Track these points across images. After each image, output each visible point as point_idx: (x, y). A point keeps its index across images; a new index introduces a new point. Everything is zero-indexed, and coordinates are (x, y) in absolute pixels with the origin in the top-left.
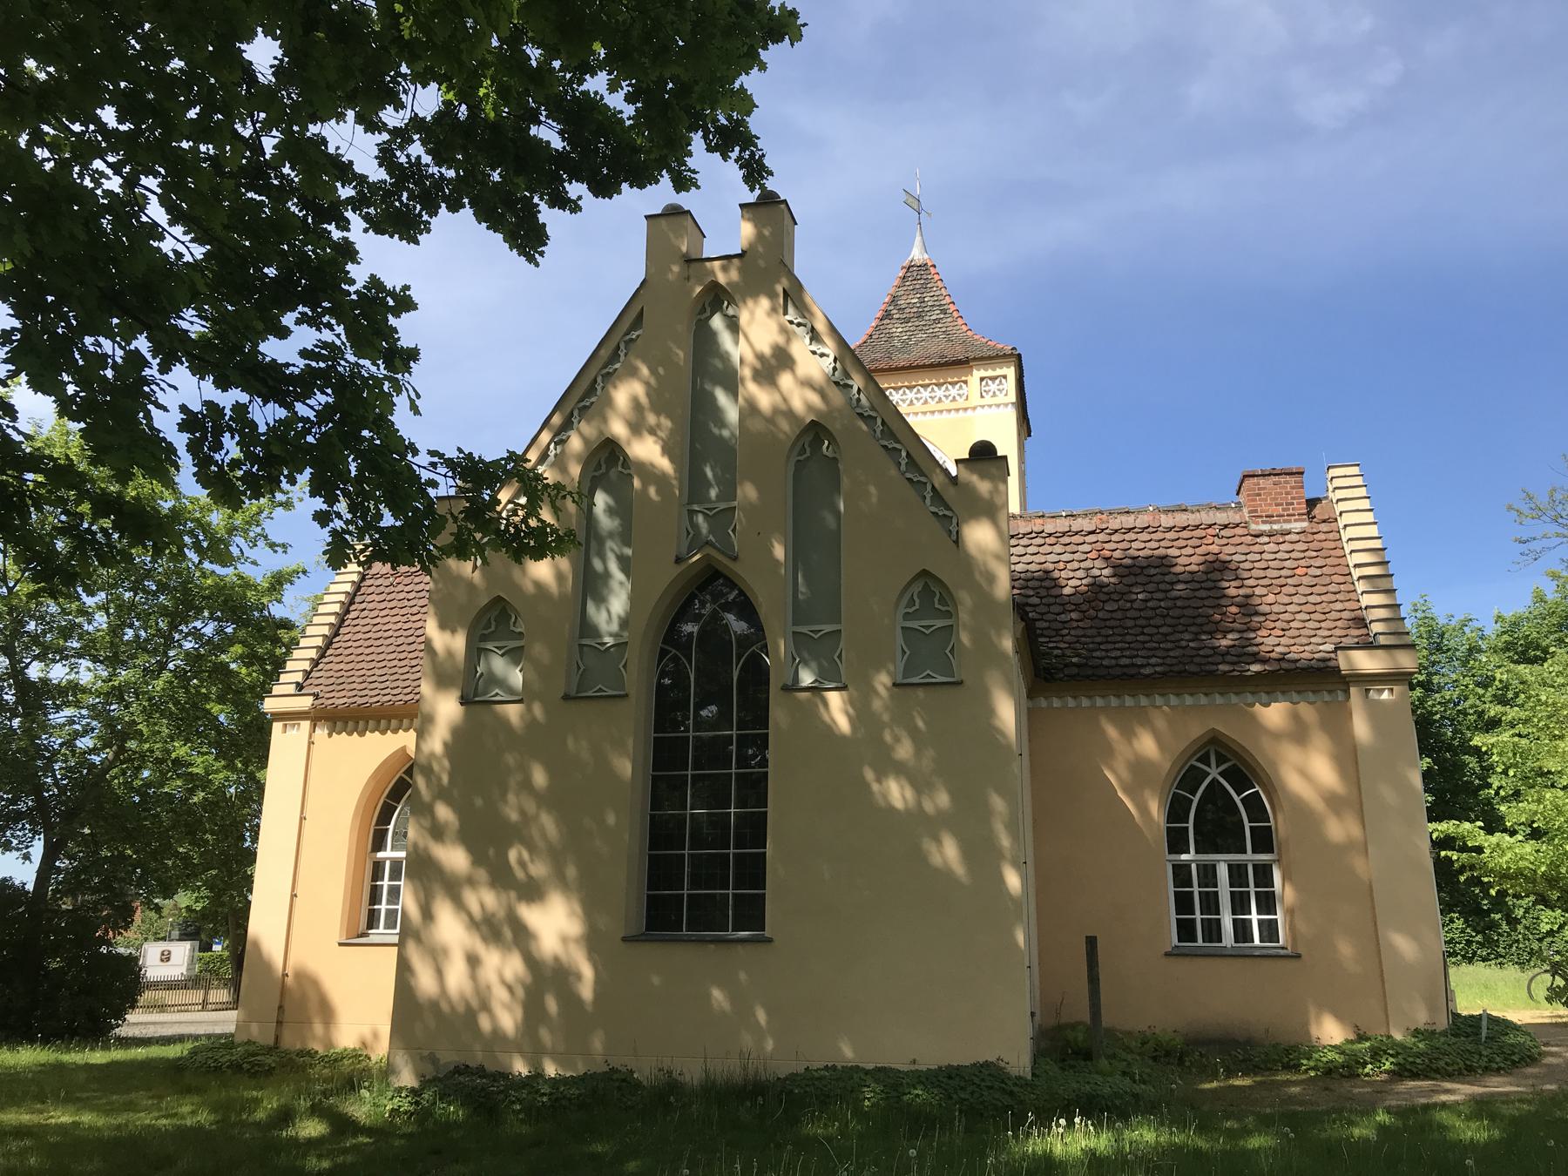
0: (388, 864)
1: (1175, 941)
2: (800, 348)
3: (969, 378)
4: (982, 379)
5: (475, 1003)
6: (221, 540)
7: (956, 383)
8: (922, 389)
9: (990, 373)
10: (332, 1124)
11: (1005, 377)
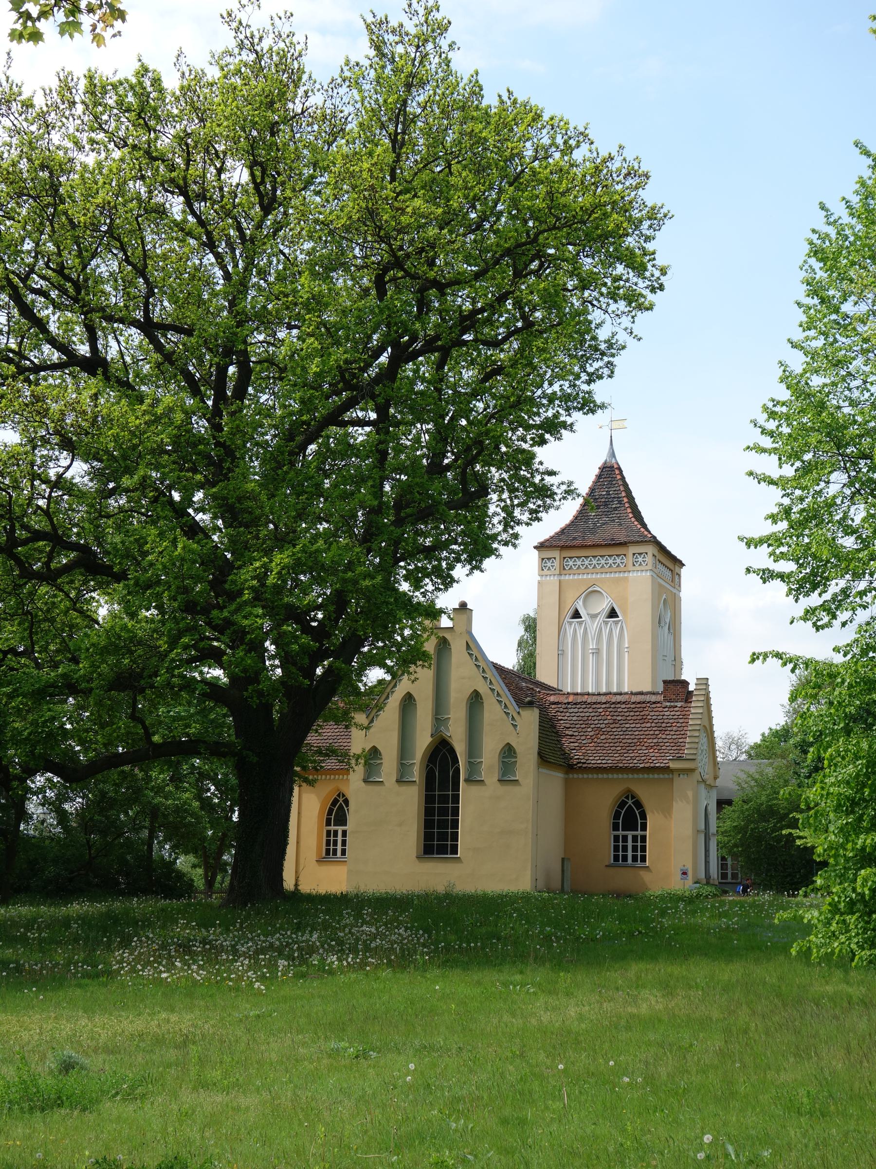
1: (612, 861)
2: (582, 375)
4: (634, 554)
6: (365, 757)
10: (522, 668)
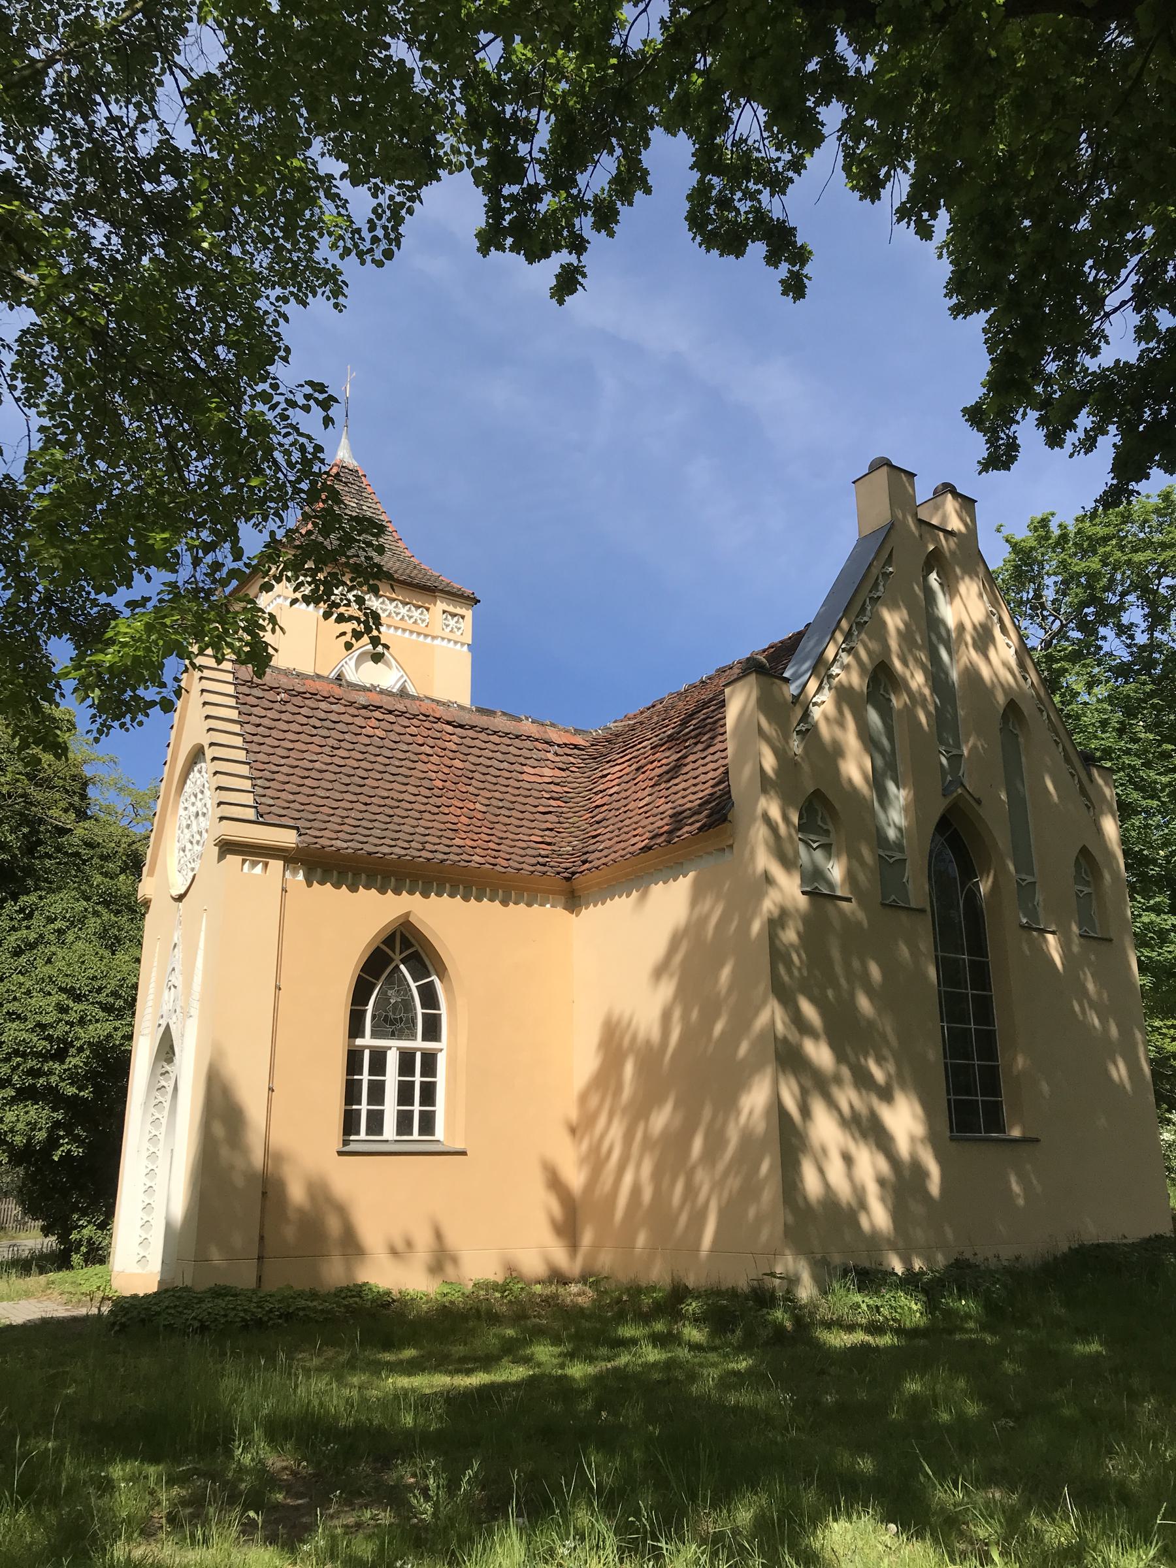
0: (367, 1053)
3: (431, 606)
5: (854, 1204)
7: (420, 607)
8: (387, 602)
9: (451, 609)
11: (463, 617)
